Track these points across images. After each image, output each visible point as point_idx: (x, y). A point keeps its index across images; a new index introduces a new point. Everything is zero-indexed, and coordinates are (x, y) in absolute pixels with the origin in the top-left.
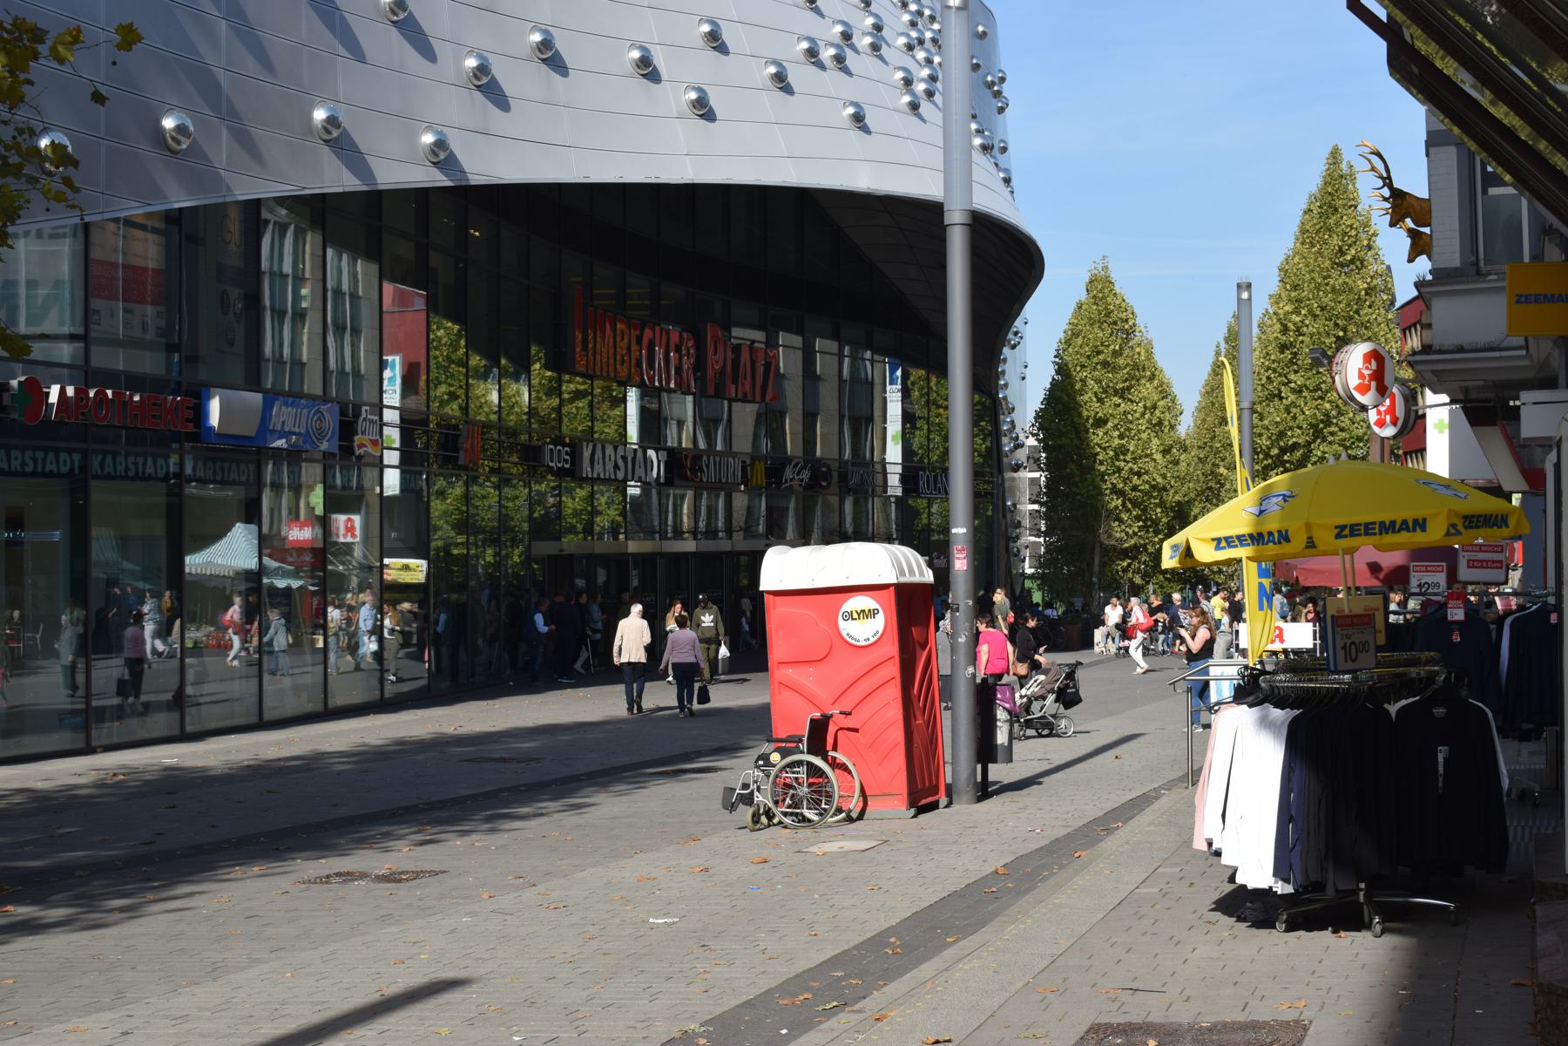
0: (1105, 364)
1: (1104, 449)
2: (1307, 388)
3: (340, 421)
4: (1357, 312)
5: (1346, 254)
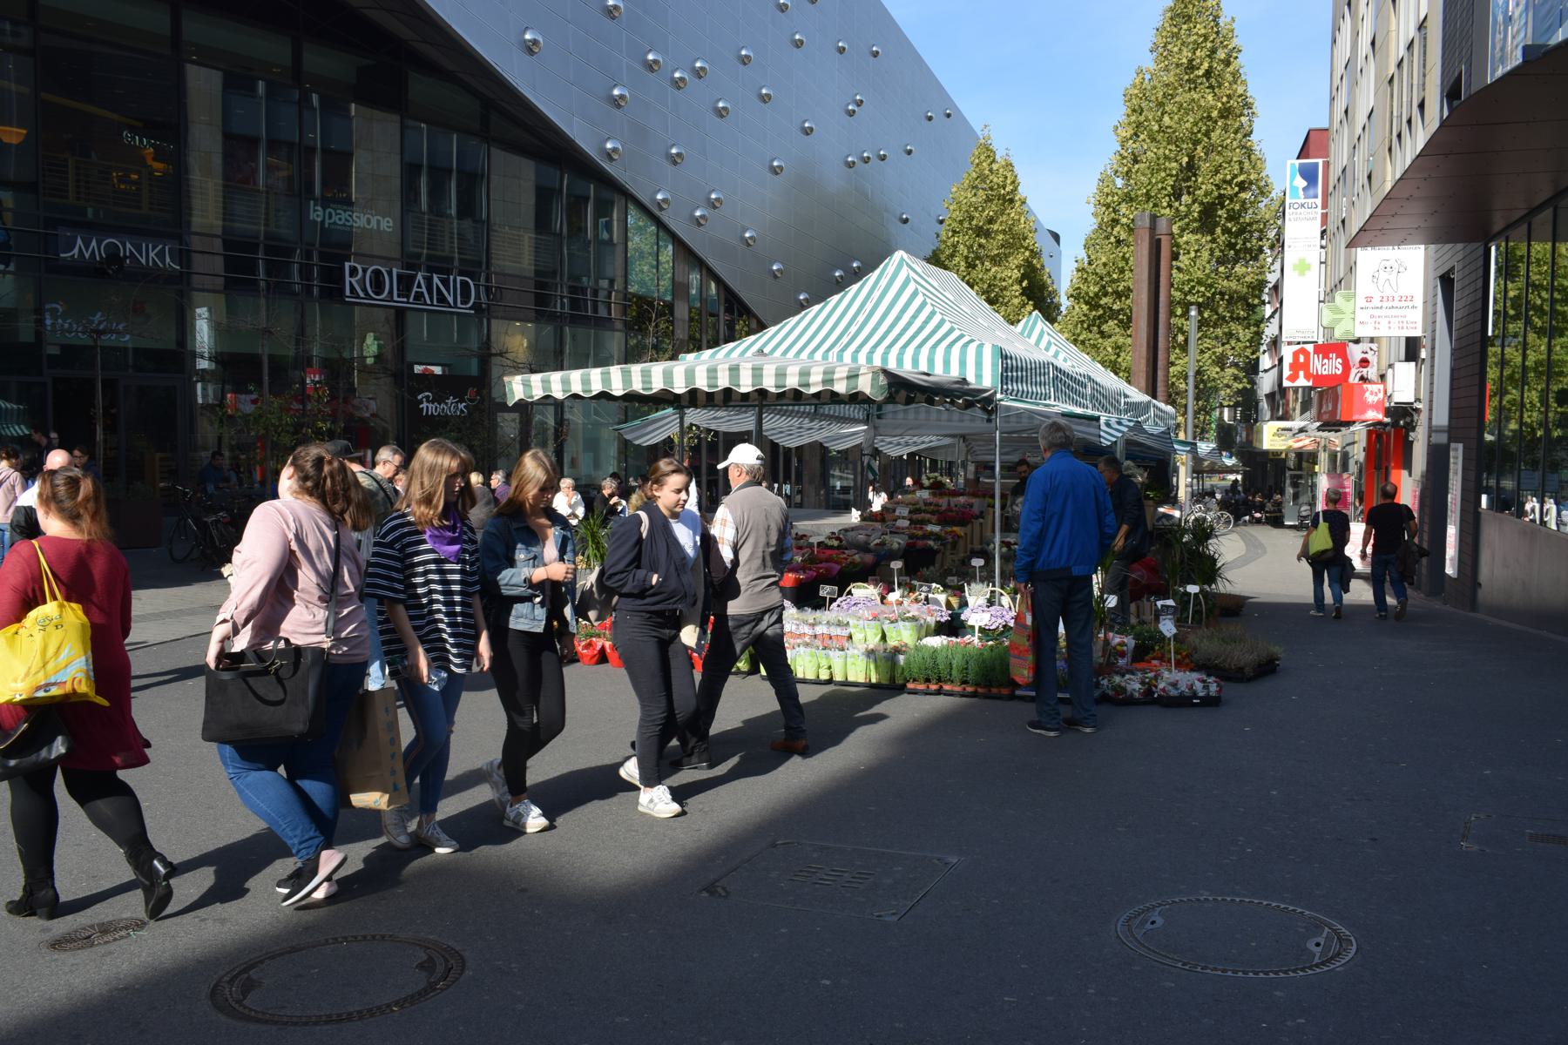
5: (1198, 68)
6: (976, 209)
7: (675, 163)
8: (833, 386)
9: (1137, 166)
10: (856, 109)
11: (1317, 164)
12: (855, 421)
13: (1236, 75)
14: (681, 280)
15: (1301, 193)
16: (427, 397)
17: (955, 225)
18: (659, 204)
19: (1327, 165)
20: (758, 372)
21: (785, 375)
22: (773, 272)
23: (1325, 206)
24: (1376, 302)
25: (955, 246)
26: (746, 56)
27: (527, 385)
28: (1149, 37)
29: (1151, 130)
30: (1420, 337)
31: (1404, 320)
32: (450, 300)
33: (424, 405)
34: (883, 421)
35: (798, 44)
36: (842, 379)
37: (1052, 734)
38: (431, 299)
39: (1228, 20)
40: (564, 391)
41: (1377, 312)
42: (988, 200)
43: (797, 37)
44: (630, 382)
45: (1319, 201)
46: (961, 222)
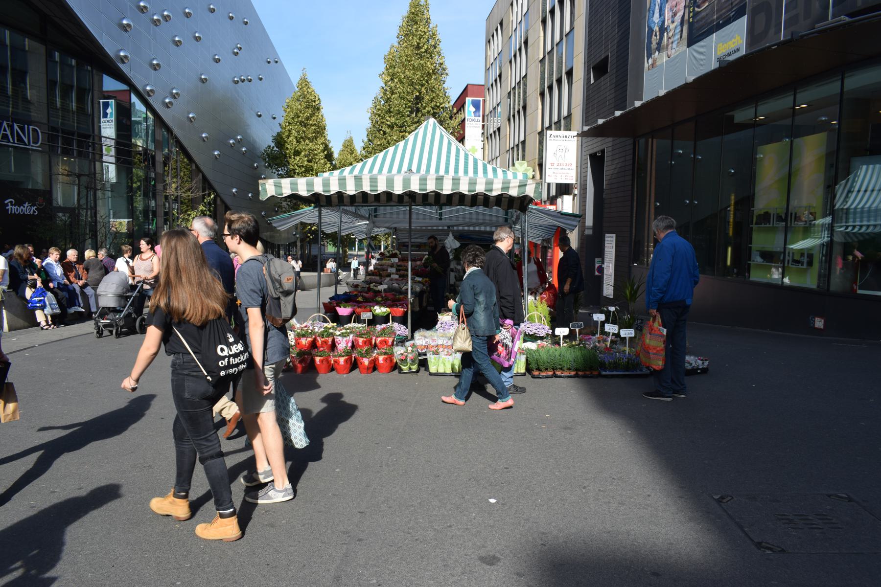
0: (301, 123)
1: (300, 167)
2: (397, 125)
3: (611, 324)
4: (427, 82)
5: (422, 48)
6: (301, 112)
7: (155, 69)
8: (508, 192)
9: (394, 96)
10: (239, 52)
11: (480, 101)
12: (362, 218)
13: (439, 53)
14: (158, 138)
15: (473, 114)
16: (11, 202)
17: (290, 120)
18: (148, 92)
19: (484, 101)
20: (456, 181)
21: (476, 183)
22: (203, 138)
23: (483, 121)
24: (555, 166)
25: (289, 131)
26: (188, 13)
27: (278, 186)
28: (395, 31)
29: (400, 78)
30: (572, 184)
31: (568, 175)
32: (26, 140)
33: (9, 207)
34: (378, 219)
35: (212, 11)
36: (515, 187)
37: (669, 399)
38: (13, 139)
39: (435, 26)
40: (308, 191)
41: (556, 171)
42: (307, 107)
43: (212, 7)
44: (361, 186)
45: (481, 118)
46: (293, 118)
